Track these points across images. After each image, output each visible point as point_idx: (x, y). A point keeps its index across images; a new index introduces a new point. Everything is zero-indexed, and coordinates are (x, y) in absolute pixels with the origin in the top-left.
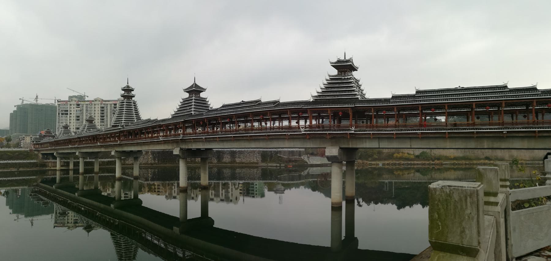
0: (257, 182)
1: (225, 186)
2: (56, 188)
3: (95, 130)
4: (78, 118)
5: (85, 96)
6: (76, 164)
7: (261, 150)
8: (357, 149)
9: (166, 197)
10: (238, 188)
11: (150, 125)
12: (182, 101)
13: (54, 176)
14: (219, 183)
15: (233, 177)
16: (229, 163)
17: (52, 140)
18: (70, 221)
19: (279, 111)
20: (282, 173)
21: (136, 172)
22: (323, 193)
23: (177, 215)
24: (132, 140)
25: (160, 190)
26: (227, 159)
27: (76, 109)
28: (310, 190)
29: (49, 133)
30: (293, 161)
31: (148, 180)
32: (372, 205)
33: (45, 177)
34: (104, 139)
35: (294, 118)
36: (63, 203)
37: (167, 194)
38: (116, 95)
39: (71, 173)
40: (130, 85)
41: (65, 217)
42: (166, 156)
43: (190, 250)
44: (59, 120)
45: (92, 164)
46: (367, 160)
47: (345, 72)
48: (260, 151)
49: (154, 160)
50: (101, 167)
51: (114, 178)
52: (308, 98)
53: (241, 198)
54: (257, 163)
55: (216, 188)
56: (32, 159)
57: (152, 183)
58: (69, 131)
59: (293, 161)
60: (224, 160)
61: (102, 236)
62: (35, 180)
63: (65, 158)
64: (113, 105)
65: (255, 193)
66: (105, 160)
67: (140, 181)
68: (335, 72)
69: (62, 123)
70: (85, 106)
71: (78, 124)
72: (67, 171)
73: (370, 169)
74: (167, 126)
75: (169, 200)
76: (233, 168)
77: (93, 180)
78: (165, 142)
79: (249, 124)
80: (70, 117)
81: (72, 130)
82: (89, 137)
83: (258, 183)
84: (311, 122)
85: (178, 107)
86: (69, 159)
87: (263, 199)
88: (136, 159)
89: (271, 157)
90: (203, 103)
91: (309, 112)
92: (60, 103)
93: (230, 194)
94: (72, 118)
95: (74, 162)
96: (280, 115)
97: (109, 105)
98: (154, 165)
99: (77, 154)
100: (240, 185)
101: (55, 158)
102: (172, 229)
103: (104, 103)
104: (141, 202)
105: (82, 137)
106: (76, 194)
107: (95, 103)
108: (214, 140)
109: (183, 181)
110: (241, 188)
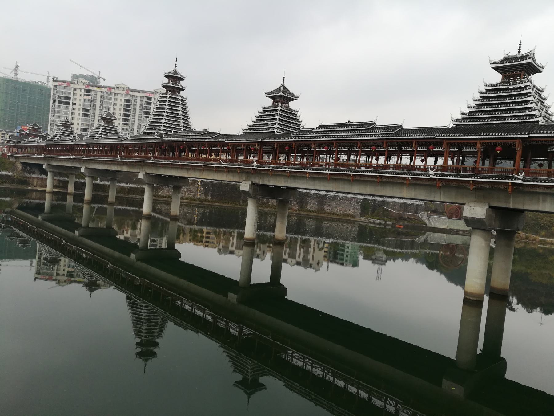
0: (349, 244)
1: (306, 244)
2: (44, 220)
3: (115, 136)
4: (86, 113)
5: (99, 78)
6: (80, 187)
7: (361, 197)
8: (523, 211)
9: (219, 251)
10: (322, 249)
11: (207, 139)
12: (261, 110)
13: (40, 201)
14: (297, 239)
15: (318, 233)
16: (315, 211)
17: (40, 142)
18: (61, 272)
19: (400, 141)
20: (388, 235)
21: (175, 209)
22: (445, 275)
23: (236, 277)
24: (174, 159)
25: (210, 240)
26: (312, 205)
27: (83, 97)
28: (424, 266)
29: (35, 132)
30: (405, 219)
31: (193, 224)
32: (537, 314)
33: (26, 200)
34: (130, 151)
35: (419, 153)
36: (54, 244)
37: (221, 247)
38: (155, 83)
39: (70, 199)
40: (179, 70)
41: (54, 265)
42: (229, 192)
43: (251, 327)
44: (54, 111)
45: (105, 189)
46: (536, 233)
47: (515, 77)
48: (360, 199)
49: (206, 194)
50: (119, 195)
51: (139, 216)
52: (445, 120)
53: (325, 264)
54: (354, 216)
55: (292, 244)
56: (5, 170)
57: (197, 228)
58: (72, 133)
59: (405, 219)
60: (309, 207)
61: (112, 301)
62: (9, 204)
63: (60, 175)
64: (145, 100)
65: (345, 258)
66: (126, 185)
67: (179, 224)
68: (497, 78)
69: (59, 117)
70: (99, 94)
71: (85, 123)
72: (63, 196)
73: (541, 251)
74: (235, 146)
75: (223, 255)
76: (320, 220)
77: (106, 214)
78: (229, 170)
79: (352, 157)
80: (73, 109)
81: (75, 131)
82: (104, 145)
83: (350, 245)
84: (446, 161)
85: (255, 119)
86: (68, 177)
87: (355, 269)
88: (177, 189)
89: (374, 209)
90: (291, 117)
91: (445, 145)
92: (56, 84)
93: (310, 257)
94: (76, 112)
95: (76, 183)
96: (400, 148)
97: (139, 99)
98: (204, 203)
99: (83, 170)
100: (326, 245)
101: (45, 173)
102: (227, 296)
103: (131, 93)
104: (179, 255)
105: (93, 145)
106: (77, 232)
107: (117, 92)
108: (301, 176)
109: (249, 231)
110: (326, 250)
